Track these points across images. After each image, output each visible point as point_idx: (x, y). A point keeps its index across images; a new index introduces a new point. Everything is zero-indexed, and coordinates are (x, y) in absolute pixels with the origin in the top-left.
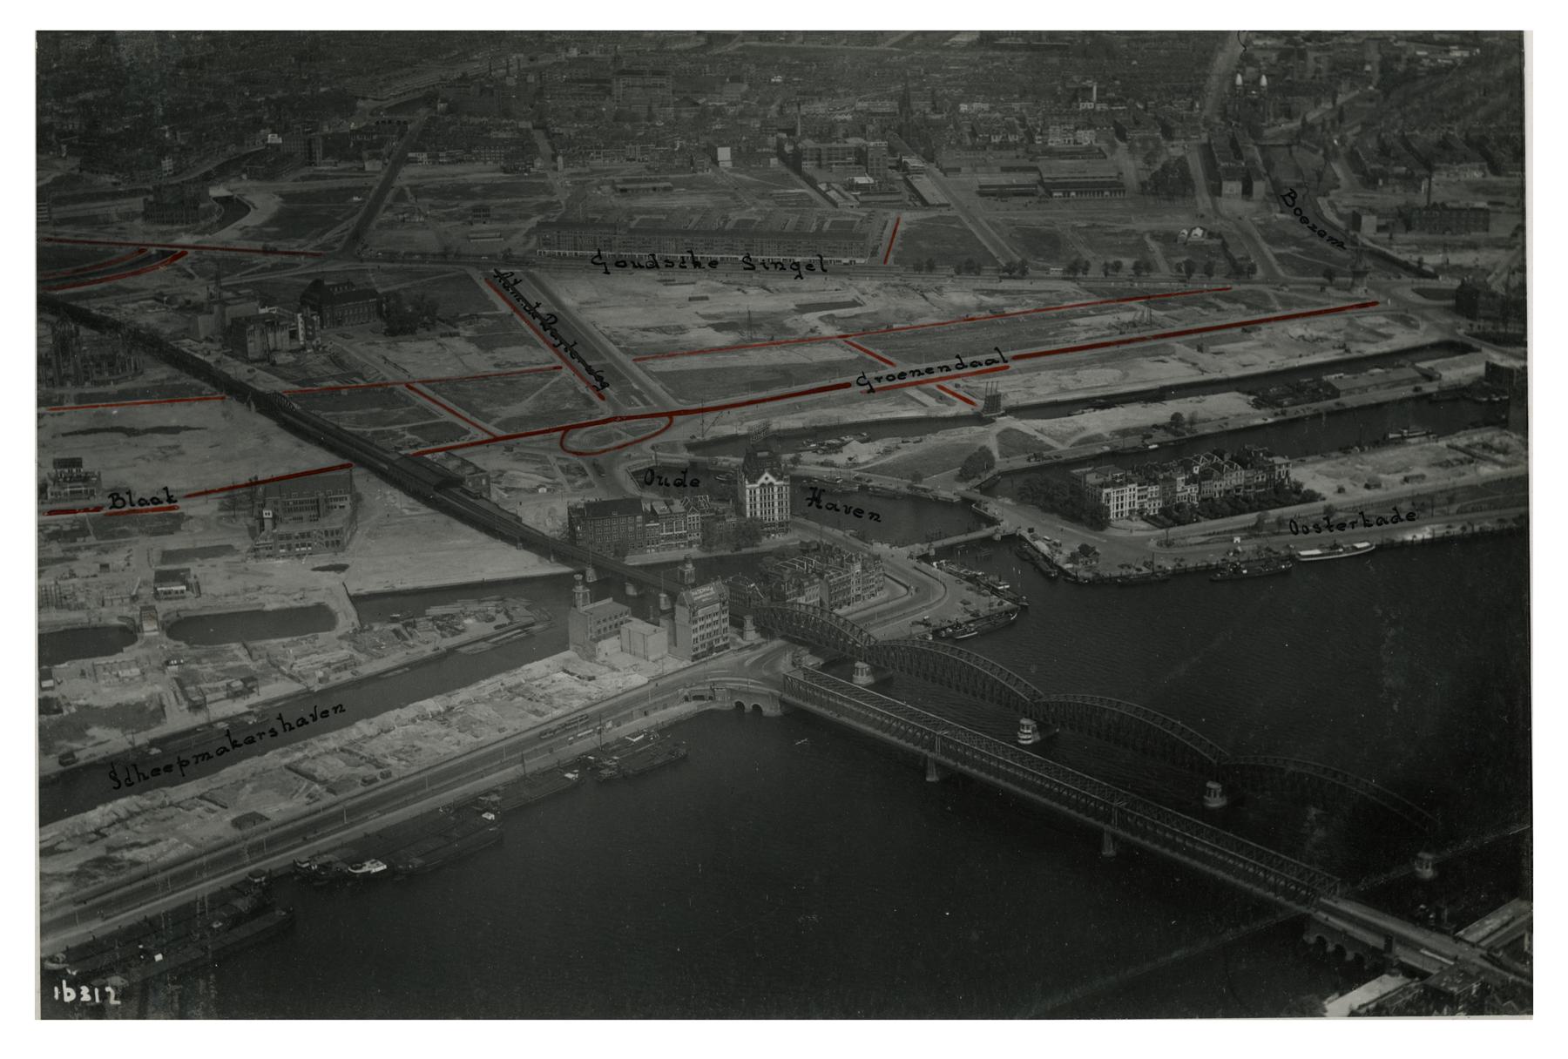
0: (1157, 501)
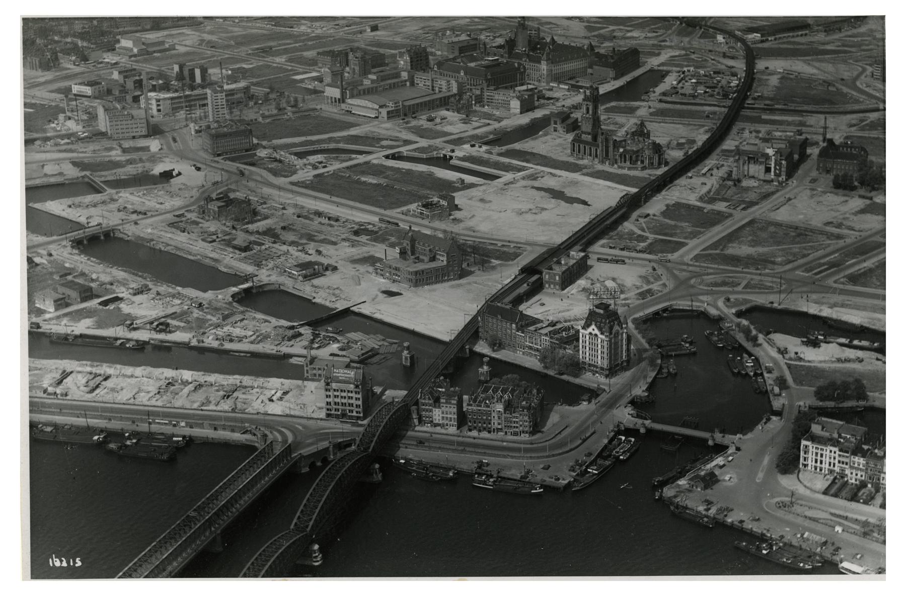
0: (859, 473)
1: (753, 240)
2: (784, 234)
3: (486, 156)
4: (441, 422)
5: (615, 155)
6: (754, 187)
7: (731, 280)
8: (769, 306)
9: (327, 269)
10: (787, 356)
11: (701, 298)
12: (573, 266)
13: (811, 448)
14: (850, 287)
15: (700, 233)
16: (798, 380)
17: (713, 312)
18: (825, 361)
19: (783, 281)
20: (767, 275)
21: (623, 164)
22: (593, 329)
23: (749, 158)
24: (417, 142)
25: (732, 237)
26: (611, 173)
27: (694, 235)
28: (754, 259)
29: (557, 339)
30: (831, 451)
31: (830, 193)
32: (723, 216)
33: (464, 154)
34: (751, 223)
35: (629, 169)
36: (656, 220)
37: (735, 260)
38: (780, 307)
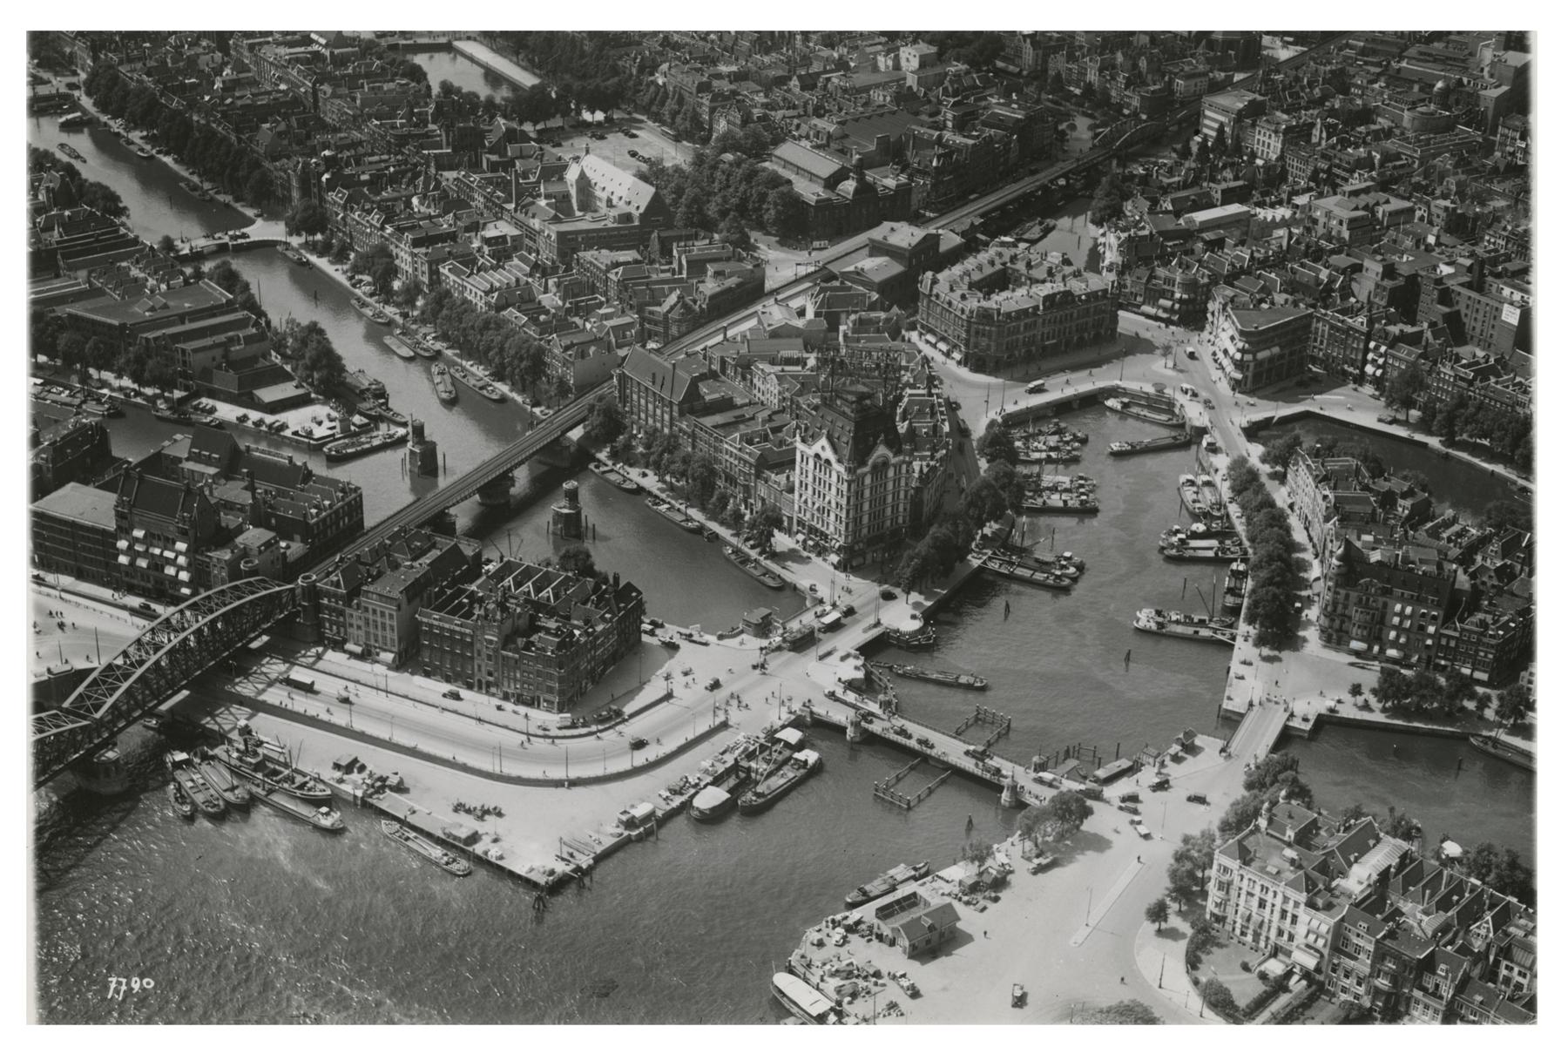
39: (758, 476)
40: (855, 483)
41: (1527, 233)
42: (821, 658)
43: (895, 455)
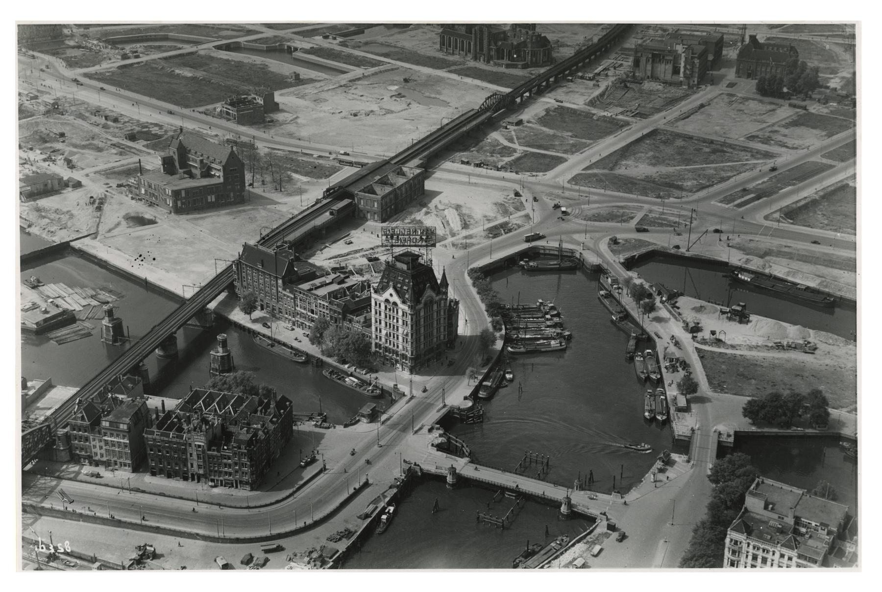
1: (654, 157)
2: (696, 150)
3: (338, 48)
4: (104, 459)
5: (490, 50)
6: (658, 90)
7: (621, 211)
8: (673, 251)
9: (66, 185)
10: (700, 335)
11: (576, 237)
12: (400, 188)
13: (744, 546)
14: (786, 226)
15: (586, 146)
16: (717, 385)
17: (592, 259)
18: (757, 347)
19: (694, 216)
20: (671, 206)
21: (500, 61)
22: (390, 294)
23: (654, 55)
24: (262, 33)
25: (625, 152)
26: (484, 71)
27: (575, 149)
28: (654, 182)
29: (338, 305)
30: (782, 556)
31: (754, 99)
32: (617, 124)
33: (311, 45)
34: (654, 133)
35: (508, 66)
36: (531, 128)
37: (628, 184)
38: (687, 254)
39: (344, 318)
40: (415, 316)
41: (855, 99)
42: (416, 432)
43: (437, 294)
